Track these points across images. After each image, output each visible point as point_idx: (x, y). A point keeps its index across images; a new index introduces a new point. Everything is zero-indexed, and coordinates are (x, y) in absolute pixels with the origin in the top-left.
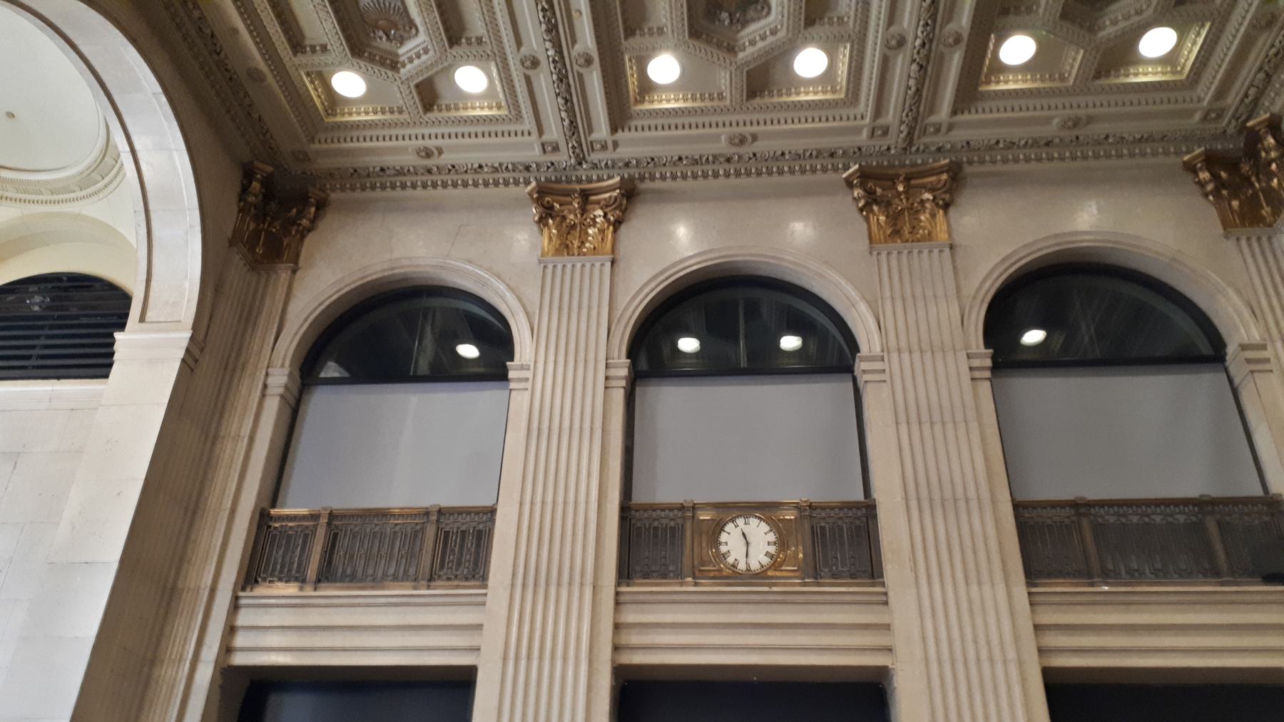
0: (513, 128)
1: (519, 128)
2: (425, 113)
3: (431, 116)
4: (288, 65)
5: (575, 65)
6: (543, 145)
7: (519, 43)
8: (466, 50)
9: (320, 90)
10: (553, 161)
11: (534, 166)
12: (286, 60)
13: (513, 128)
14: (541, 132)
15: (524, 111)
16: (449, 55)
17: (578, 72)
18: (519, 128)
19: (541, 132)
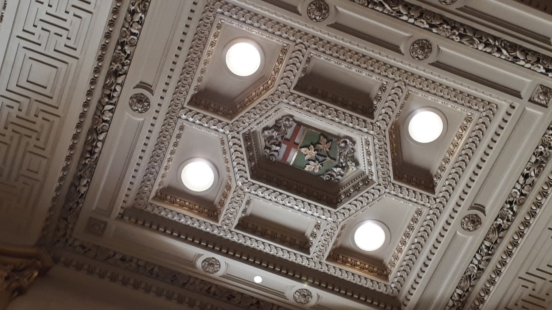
0: (498, 120)
1: (501, 114)
2: (309, 254)
3: (440, 185)
4: (312, 265)
5: (448, 7)
6: (530, 100)
7: (396, 49)
8: (383, 106)
9: (358, 263)
10: (183, 66)
11: (500, 221)
12: (305, 263)
13: (498, 120)
14: (517, 94)
15: (487, 98)
16: (378, 123)
17: (460, 9)
18: (501, 114)
19: (517, 94)
